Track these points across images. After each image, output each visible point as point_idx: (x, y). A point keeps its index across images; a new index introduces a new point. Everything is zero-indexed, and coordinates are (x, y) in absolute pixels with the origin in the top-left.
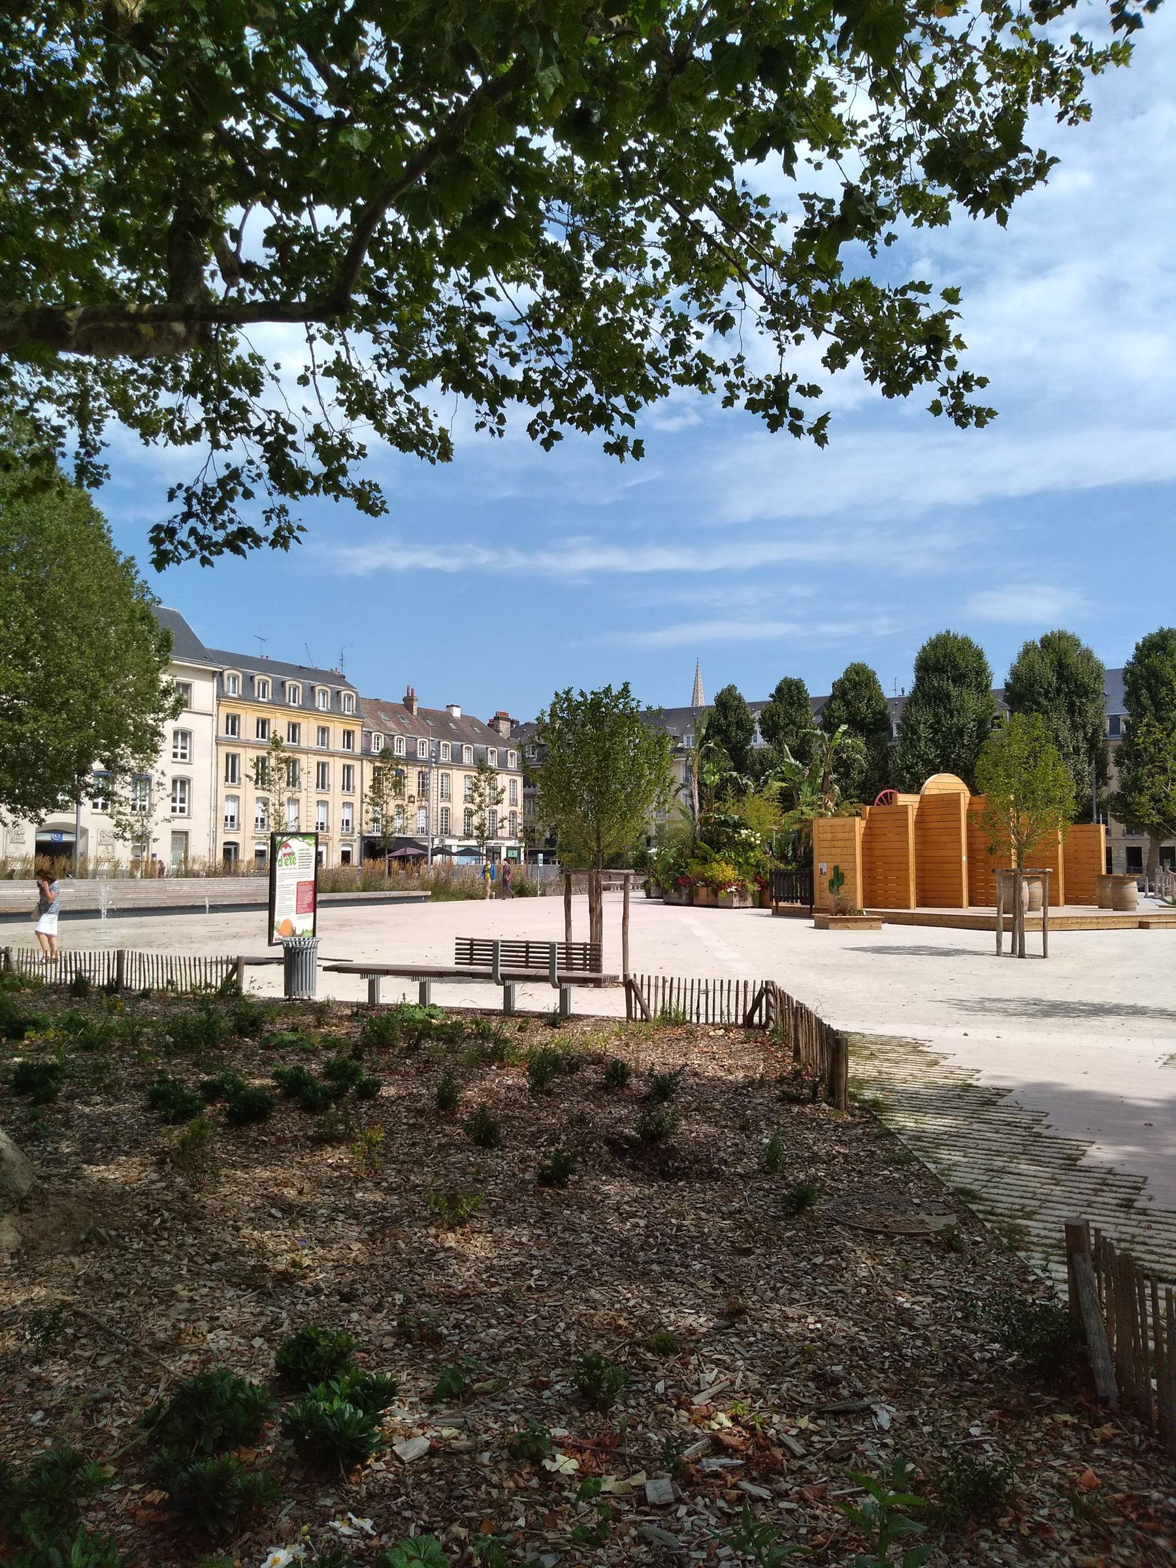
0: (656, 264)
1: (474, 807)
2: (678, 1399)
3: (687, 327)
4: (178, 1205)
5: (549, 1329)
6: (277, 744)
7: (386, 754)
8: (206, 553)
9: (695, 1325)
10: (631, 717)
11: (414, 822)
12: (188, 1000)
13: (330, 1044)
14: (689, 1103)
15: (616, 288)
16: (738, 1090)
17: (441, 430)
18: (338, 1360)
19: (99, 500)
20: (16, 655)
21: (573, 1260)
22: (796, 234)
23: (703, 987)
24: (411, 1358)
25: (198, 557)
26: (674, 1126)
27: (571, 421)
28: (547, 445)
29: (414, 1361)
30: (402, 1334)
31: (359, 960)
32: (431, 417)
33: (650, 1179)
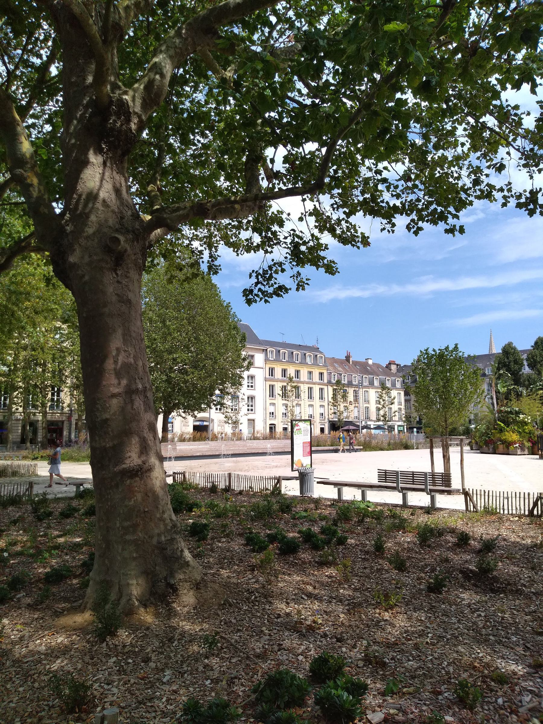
0: (463, 145)
1: (380, 406)
2: (511, 709)
3: (481, 171)
4: (261, 590)
5: (439, 665)
6: (291, 379)
7: (338, 382)
8: (267, 298)
9: (516, 670)
10: (460, 360)
11: (352, 414)
12: (259, 495)
13: (323, 518)
14: (502, 554)
15: (444, 158)
16: (528, 548)
17: (362, 233)
18: (338, 670)
19: (215, 279)
20: (184, 346)
21: (448, 630)
22: (536, 121)
23: (506, 495)
24: (372, 673)
25: (263, 300)
26: (496, 566)
27: (427, 221)
28: (416, 233)
29: (373, 674)
30: (367, 660)
31: (332, 479)
32: (357, 228)
33: (485, 592)
